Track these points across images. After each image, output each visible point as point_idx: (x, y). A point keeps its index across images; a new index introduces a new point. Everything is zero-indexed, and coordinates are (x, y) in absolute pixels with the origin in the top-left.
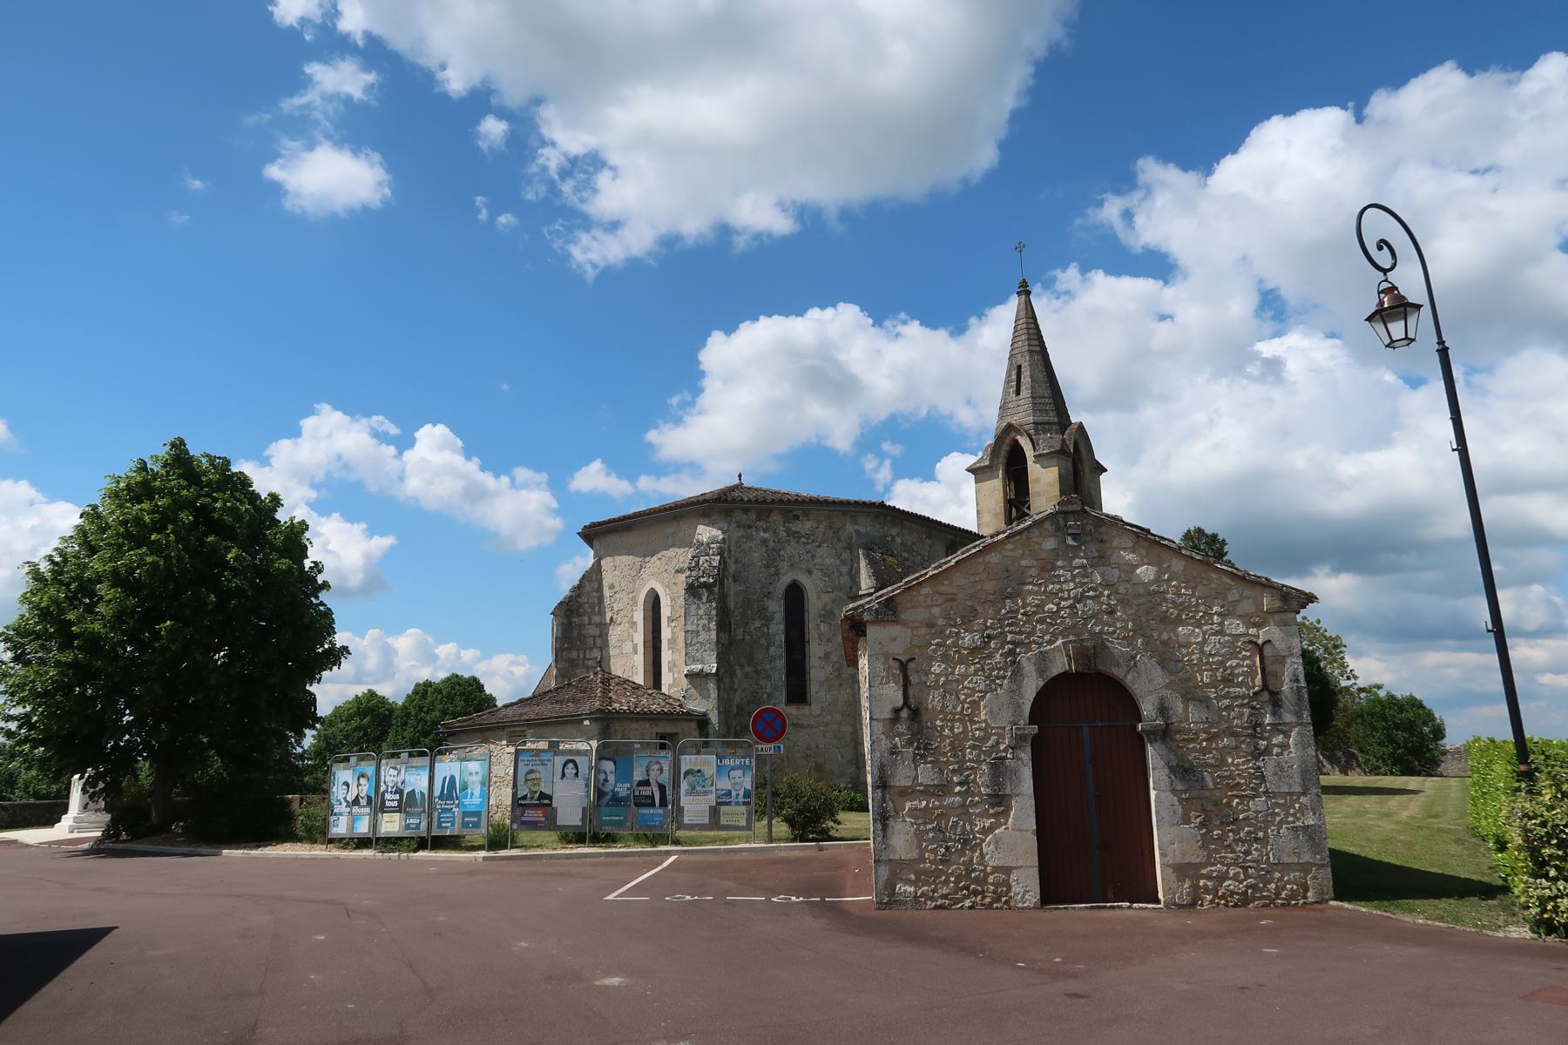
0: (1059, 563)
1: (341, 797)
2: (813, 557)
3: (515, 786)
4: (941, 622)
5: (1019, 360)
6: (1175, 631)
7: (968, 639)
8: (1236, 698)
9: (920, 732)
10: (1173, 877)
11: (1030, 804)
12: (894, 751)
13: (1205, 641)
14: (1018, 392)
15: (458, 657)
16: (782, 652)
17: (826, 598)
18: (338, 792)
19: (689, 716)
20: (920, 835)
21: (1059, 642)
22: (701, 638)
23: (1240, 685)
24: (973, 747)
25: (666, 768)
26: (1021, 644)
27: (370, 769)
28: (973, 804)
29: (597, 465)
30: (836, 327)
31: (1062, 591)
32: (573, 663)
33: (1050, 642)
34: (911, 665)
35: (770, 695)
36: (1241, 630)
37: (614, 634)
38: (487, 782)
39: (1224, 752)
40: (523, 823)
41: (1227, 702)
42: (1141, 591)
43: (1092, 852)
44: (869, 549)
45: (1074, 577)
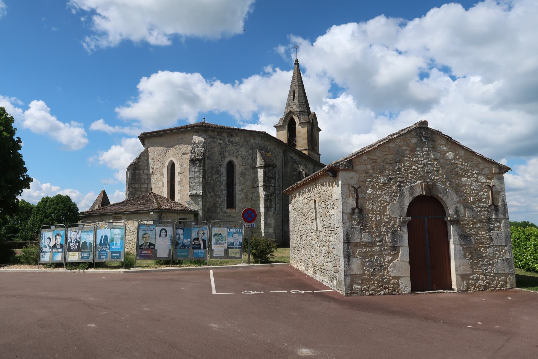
0: (418, 149)
1: (46, 244)
2: (238, 151)
3: (138, 240)
4: (371, 171)
5: (294, 88)
6: (460, 179)
7: (382, 179)
8: (483, 207)
9: (363, 219)
10: (460, 279)
11: (407, 250)
12: (352, 227)
13: (471, 184)
14: (293, 100)
15: (51, 189)
16: (225, 188)
17: (242, 167)
18: (44, 242)
19: (191, 211)
20: (363, 264)
21: (418, 182)
22: (196, 181)
23: (484, 202)
24: (384, 226)
25: (206, 232)
26: (403, 182)
27: (62, 232)
28: (385, 250)
29: (101, 121)
30: (195, 80)
31: (419, 161)
32: (136, 189)
33: (415, 182)
34: (359, 190)
35: (220, 204)
36: (484, 180)
37: (154, 178)
38: (123, 238)
39: (479, 229)
40: (142, 256)
41: (479, 209)
42: (449, 162)
43: (429, 272)
44: (260, 150)
45: (423, 155)
